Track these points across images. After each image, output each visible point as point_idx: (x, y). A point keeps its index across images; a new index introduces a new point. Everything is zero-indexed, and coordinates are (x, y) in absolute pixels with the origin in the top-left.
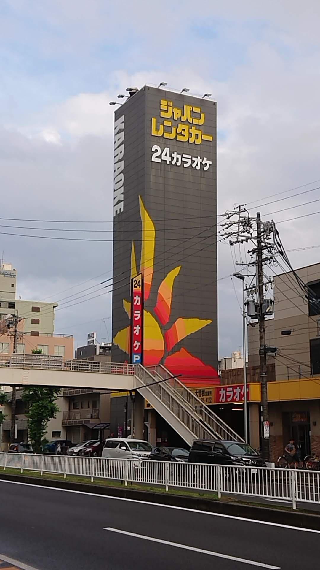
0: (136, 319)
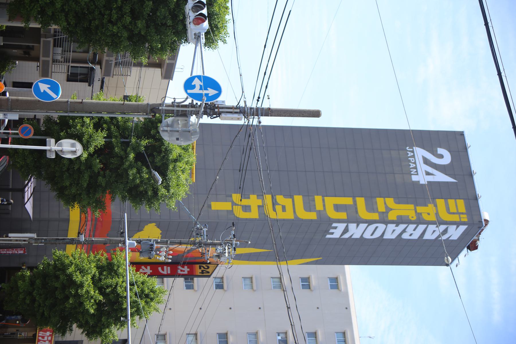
0: (160, 269)
